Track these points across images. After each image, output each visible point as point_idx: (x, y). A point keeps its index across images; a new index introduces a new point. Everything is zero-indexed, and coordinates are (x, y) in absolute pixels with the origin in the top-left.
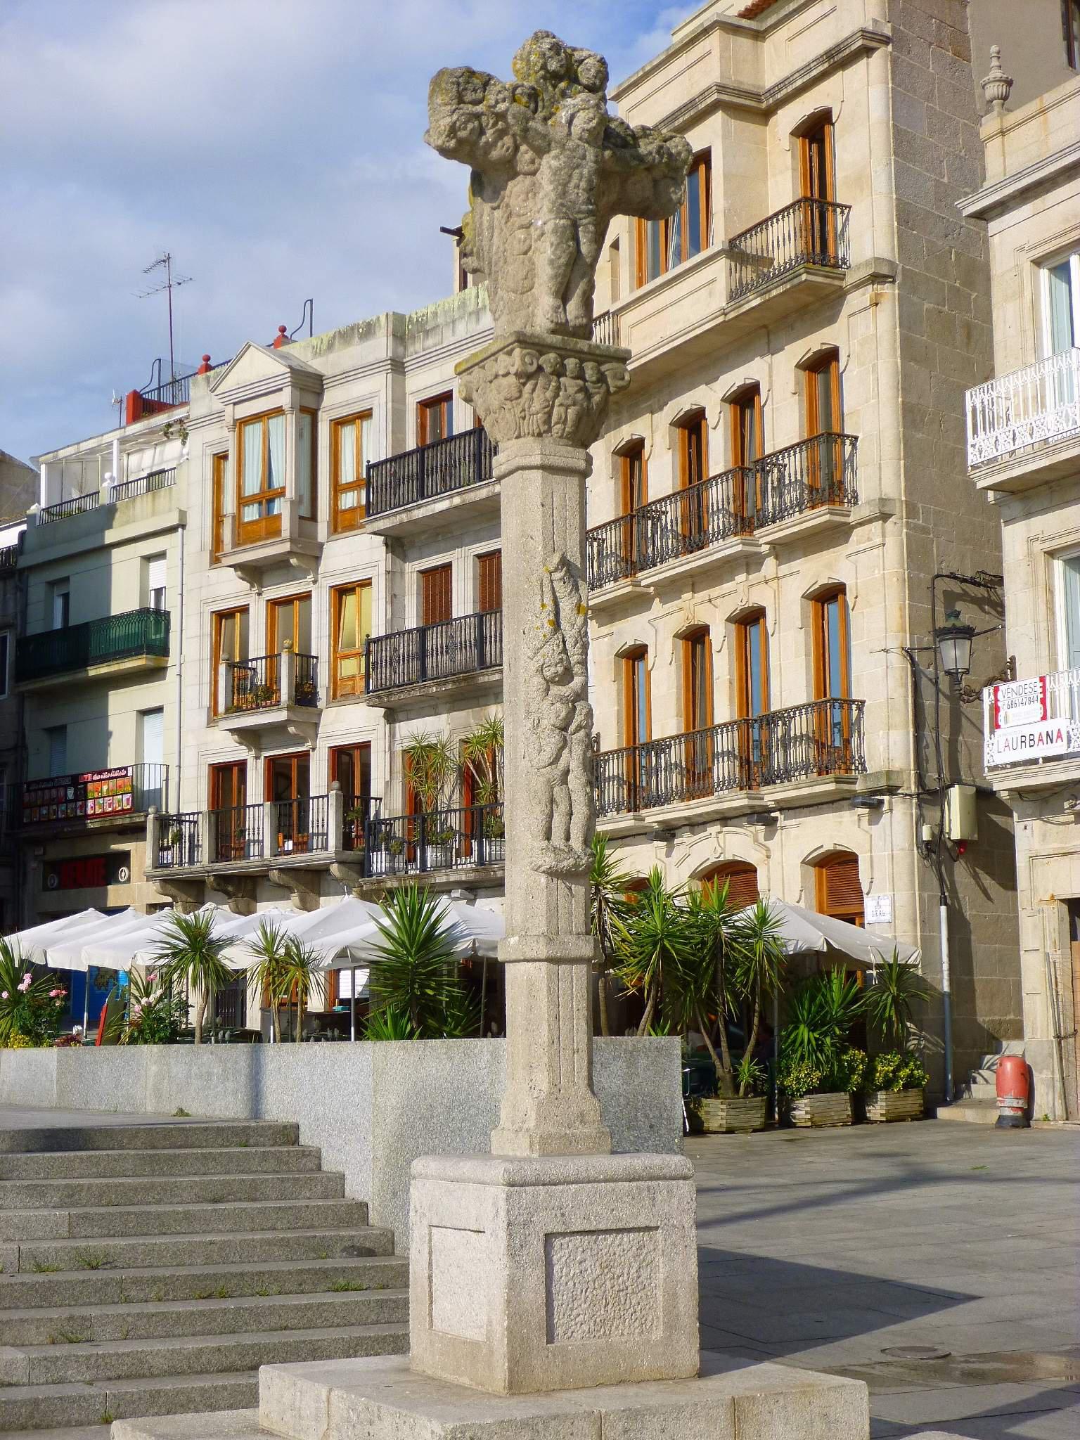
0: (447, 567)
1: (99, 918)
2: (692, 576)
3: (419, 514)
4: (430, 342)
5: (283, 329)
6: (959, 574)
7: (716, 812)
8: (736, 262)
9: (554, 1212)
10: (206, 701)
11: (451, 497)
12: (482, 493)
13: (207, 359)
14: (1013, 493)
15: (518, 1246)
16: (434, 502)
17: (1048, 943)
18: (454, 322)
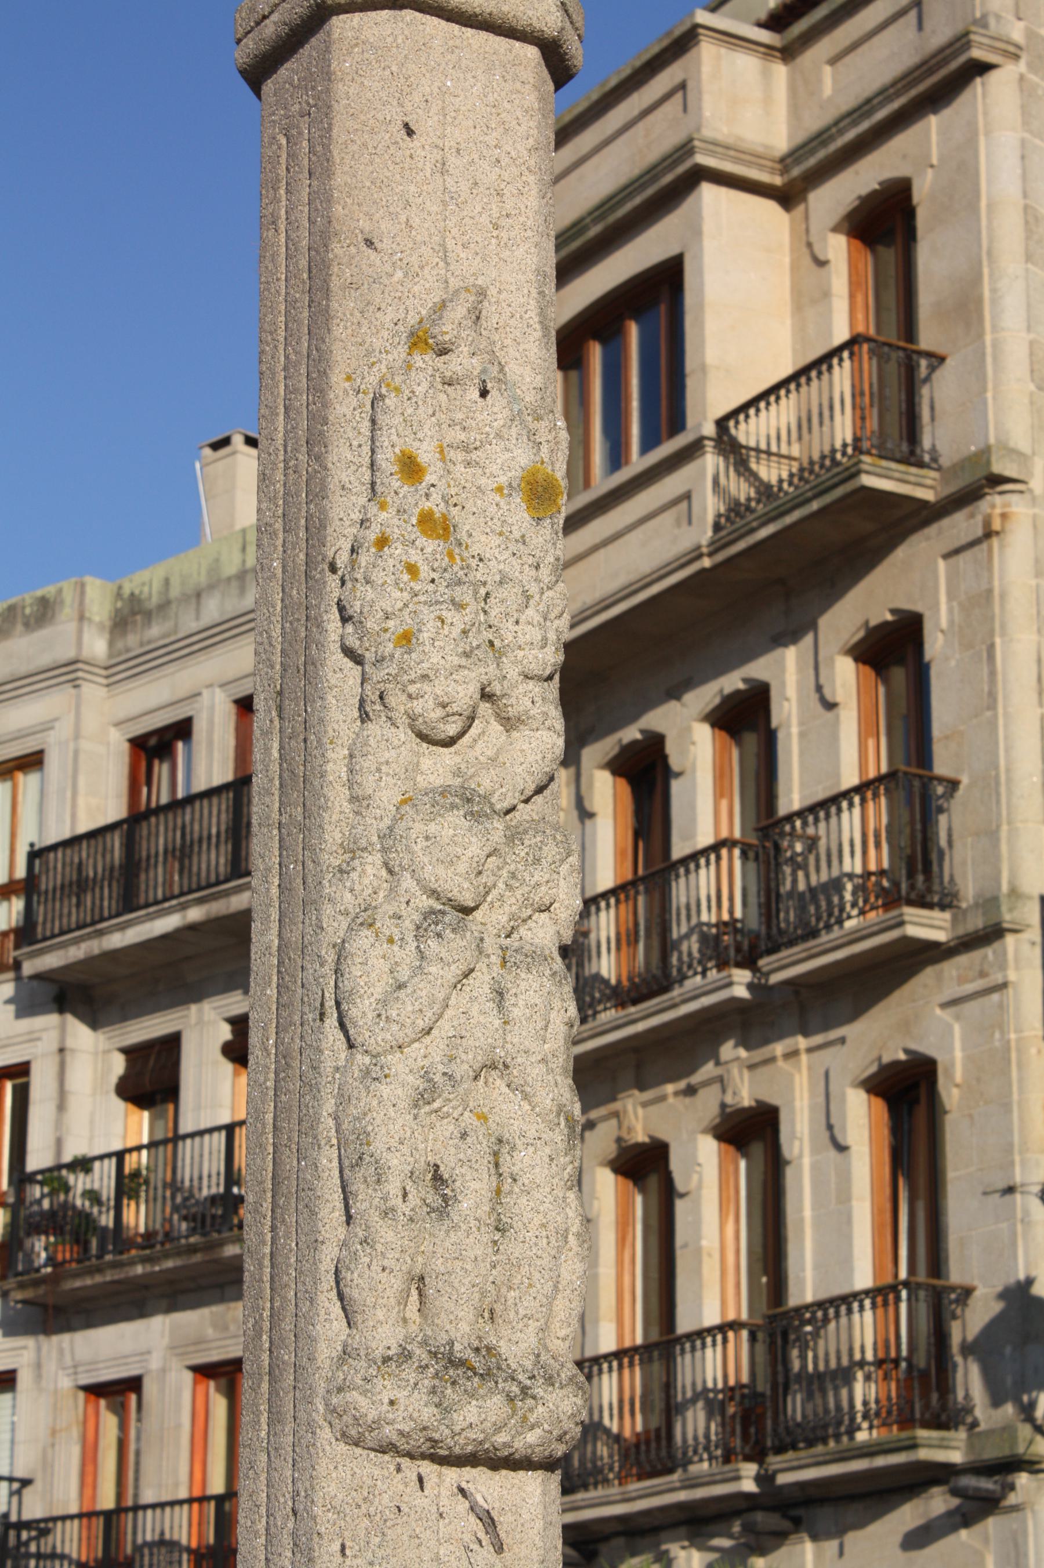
0: (171, 1044)
1: (975, 88)
2: (636, 1050)
3: (117, 940)
4: (155, 630)
7: (680, 1506)
8: (726, 458)
12: (237, 902)
16: (150, 918)
18: (198, 595)
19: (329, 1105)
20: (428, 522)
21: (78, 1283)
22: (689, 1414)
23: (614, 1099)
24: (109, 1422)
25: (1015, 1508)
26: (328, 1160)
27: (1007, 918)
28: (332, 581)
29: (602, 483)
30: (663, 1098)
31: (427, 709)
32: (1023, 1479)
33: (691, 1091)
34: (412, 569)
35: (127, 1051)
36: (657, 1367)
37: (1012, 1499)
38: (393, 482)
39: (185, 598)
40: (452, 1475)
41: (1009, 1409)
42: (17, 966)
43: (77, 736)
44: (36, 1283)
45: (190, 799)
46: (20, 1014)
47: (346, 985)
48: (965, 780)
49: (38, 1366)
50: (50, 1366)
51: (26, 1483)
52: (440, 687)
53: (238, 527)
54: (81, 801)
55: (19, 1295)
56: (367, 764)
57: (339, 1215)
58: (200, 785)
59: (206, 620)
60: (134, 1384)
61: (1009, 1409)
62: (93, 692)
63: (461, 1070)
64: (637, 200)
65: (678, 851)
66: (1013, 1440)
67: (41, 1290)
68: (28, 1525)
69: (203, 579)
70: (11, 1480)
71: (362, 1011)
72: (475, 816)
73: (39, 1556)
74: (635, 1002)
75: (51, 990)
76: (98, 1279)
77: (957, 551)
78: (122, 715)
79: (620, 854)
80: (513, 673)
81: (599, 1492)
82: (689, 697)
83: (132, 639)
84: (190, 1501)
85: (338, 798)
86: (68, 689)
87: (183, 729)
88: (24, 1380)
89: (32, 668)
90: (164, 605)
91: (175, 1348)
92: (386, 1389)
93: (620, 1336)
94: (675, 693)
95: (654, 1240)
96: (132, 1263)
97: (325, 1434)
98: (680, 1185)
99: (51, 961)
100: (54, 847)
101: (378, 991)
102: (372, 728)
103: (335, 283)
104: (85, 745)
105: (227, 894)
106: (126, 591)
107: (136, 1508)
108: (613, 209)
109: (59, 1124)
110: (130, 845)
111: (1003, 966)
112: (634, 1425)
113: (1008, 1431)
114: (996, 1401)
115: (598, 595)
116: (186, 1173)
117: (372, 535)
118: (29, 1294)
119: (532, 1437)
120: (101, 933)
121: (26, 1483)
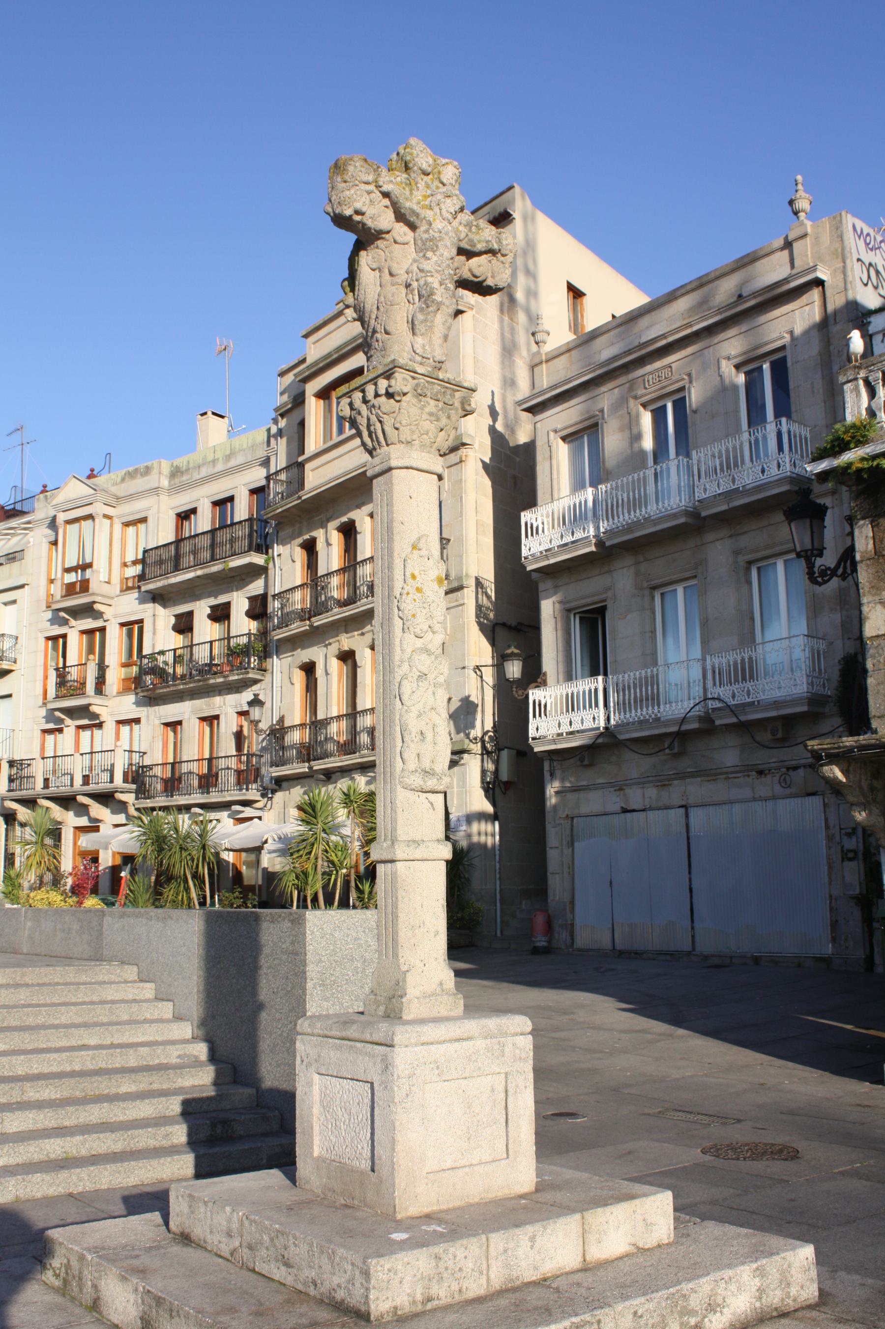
0: (190, 614)
3: (173, 580)
4: (184, 478)
5: (92, 470)
6: (509, 623)
9: (431, 1066)
10: (40, 691)
11: (196, 570)
13: (45, 486)
14: (547, 574)
15: (404, 1095)
16: (184, 573)
17: (564, 843)
19: (398, 717)
20: (419, 590)
21: (161, 691)
22: (362, 735)
23: (337, 636)
24: (171, 734)
25: (463, 765)
26: (398, 729)
27: (465, 583)
28: (396, 601)
29: (336, 439)
30: (354, 636)
31: (418, 631)
32: (466, 756)
33: (363, 634)
34: (415, 600)
35: (176, 616)
36: (351, 721)
37: (462, 762)
38: (409, 580)
39: (195, 468)
40: (425, 795)
41: (462, 735)
42: (139, 587)
43: (158, 512)
44: (147, 690)
45: (197, 535)
46: (140, 603)
47: (401, 691)
48: (452, 539)
49: (148, 716)
50: (152, 717)
51: (145, 753)
52: (421, 626)
53: (211, 444)
54: (160, 534)
55: (142, 694)
56: (405, 642)
57: (400, 741)
58: (200, 531)
59: (201, 475)
60: (180, 723)
61: (462, 735)
62: (164, 498)
63: (426, 710)
64: (349, 347)
65: (359, 559)
66: (463, 744)
67: (149, 693)
68: (146, 767)
69: (201, 462)
70: (140, 752)
71: (405, 698)
72: (429, 655)
73: (150, 776)
74: (345, 606)
75: (150, 596)
76: (168, 689)
77: (451, 466)
78: (173, 506)
79: (340, 557)
80: (435, 622)
81: (332, 759)
82: (363, 508)
83: (177, 481)
84: (198, 760)
85: (398, 649)
86: (155, 496)
87: (194, 511)
88: (143, 721)
89: (143, 489)
90: (188, 470)
91: (193, 712)
92: (412, 778)
93: (339, 711)
94: (359, 507)
95: (350, 681)
96: (179, 685)
97: (399, 787)
98: (359, 664)
99: (151, 586)
100: (151, 549)
101: (409, 693)
102: (405, 635)
103: (395, 532)
104: (161, 515)
105: (210, 566)
106: (175, 465)
107: (181, 762)
108: (342, 349)
109: (153, 639)
110: (177, 549)
111: (463, 598)
112: (343, 738)
113: (462, 741)
114: (458, 732)
115: (335, 475)
116: (196, 656)
117: (405, 592)
118: (145, 694)
119: (442, 787)
120: (168, 578)
121: (145, 753)
